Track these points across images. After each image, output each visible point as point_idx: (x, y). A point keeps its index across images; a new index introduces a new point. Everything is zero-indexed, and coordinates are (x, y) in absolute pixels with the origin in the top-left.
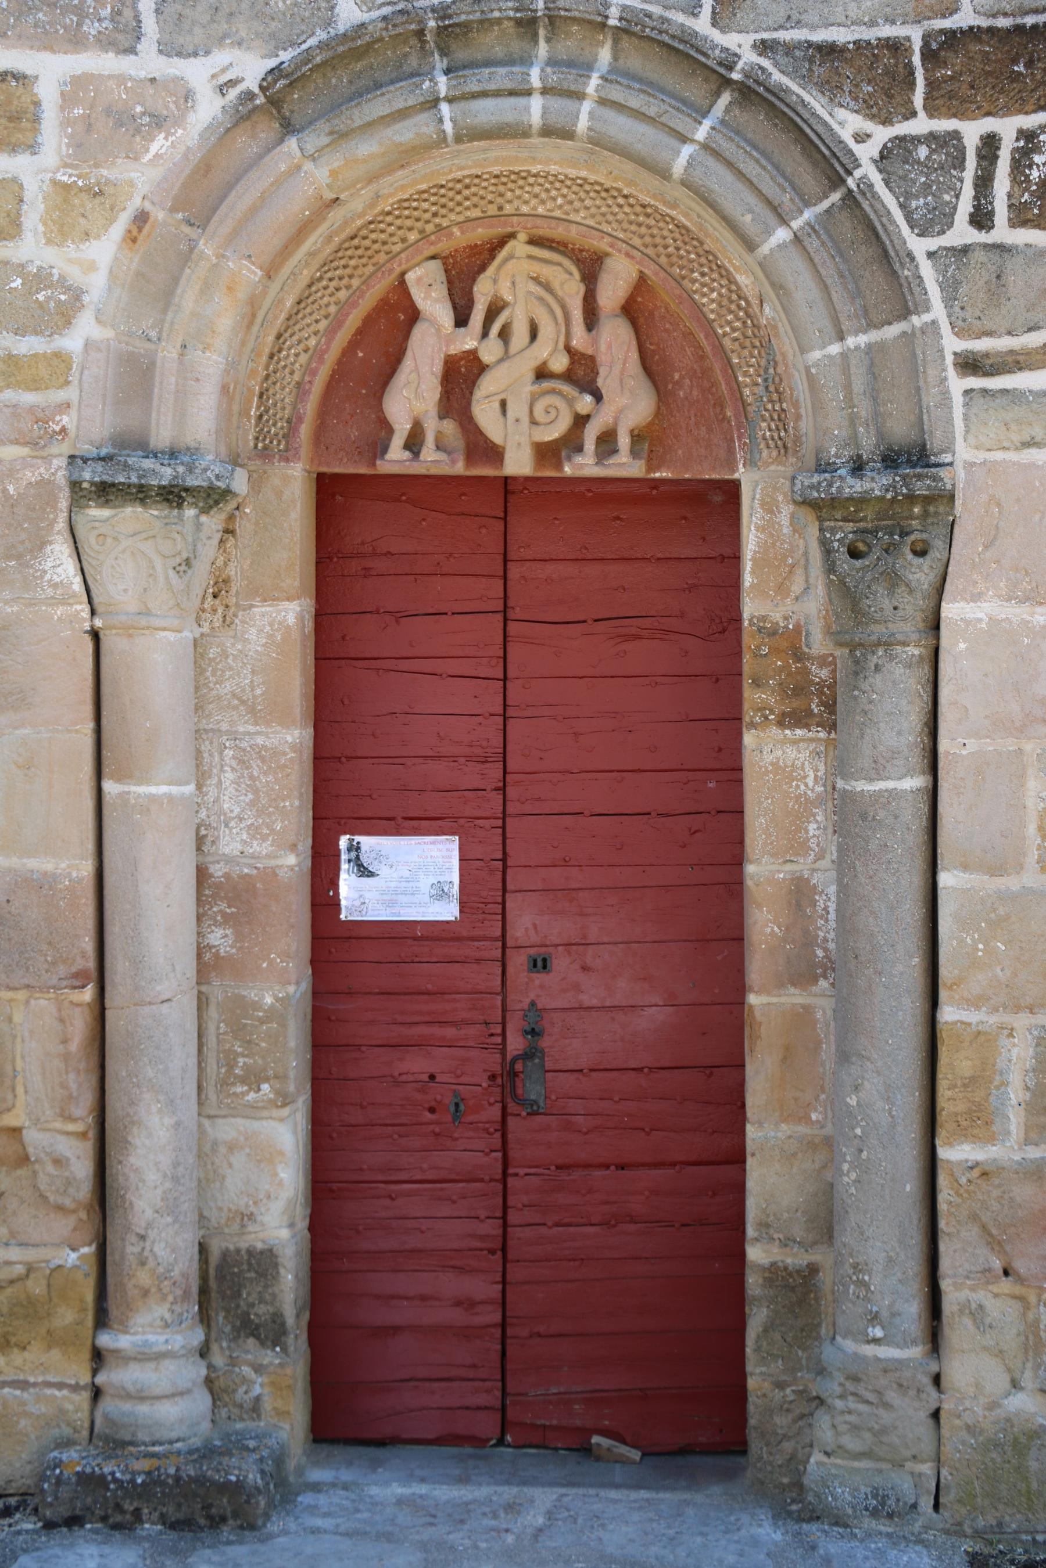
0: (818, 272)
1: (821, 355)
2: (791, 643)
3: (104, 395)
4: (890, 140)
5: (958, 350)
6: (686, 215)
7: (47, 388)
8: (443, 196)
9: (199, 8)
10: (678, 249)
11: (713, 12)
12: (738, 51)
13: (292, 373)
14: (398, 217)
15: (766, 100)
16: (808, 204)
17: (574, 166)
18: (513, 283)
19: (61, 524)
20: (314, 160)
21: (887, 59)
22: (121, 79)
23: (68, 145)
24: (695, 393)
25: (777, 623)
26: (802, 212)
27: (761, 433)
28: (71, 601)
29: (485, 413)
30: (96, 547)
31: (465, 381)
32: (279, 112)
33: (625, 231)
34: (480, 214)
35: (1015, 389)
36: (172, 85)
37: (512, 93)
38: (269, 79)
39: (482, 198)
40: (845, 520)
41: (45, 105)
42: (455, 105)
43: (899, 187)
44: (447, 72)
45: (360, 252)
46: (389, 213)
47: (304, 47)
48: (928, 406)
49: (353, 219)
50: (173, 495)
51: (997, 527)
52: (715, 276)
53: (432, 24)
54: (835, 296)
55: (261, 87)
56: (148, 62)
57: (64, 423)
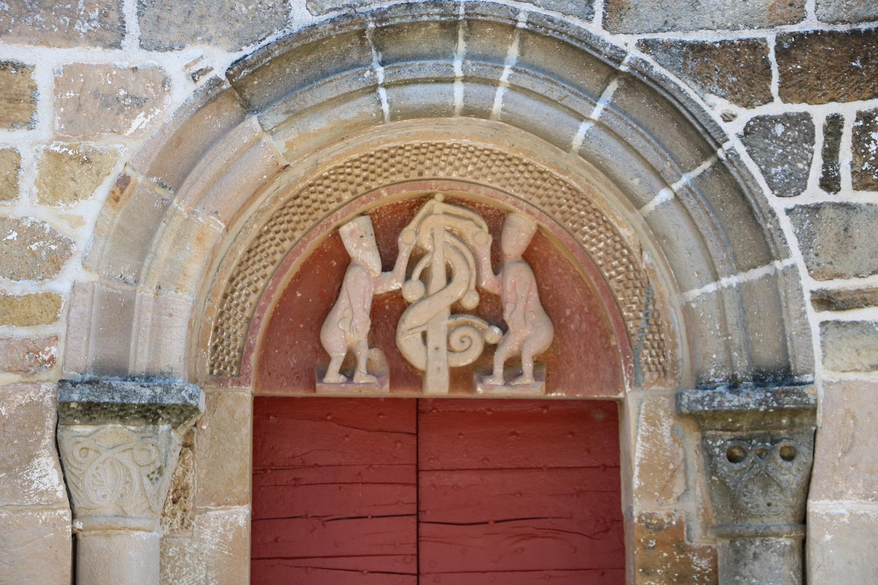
0: (695, 224)
1: (696, 295)
2: (674, 536)
3: (89, 329)
4: (752, 120)
5: (814, 289)
6: (577, 180)
7: (37, 324)
8: (372, 164)
9: (175, 12)
10: (570, 207)
11: (604, 18)
12: (625, 48)
13: (243, 310)
14: (334, 181)
15: (648, 87)
16: (684, 170)
17: (482, 140)
18: (432, 235)
19: (48, 440)
20: (272, 134)
21: (748, 56)
22: (108, 69)
23: (61, 122)
24: (584, 326)
25: (662, 520)
26: (681, 177)
27: (644, 359)
28: (55, 507)
29: (409, 344)
30: (80, 459)
31: (389, 316)
32: (241, 95)
33: (526, 192)
34: (403, 179)
35: (863, 321)
36: (151, 73)
37: (438, 81)
38: (235, 68)
39: (406, 165)
40: (724, 429)
41: (40, 89)
42: (391, 90)
43: (761, 157)
44: (383, 63)
45: (301, 210)
46: (326, 178)
47: (264, 43)
48: (791, 335)
49: (296, 183)
50: (150, 413)
51: (853, 436)
52: (602, 229)
53: (371, 25)
54: (709, 244)
55: (227, 75)
56: (130, 54)
57: (52, 353)
